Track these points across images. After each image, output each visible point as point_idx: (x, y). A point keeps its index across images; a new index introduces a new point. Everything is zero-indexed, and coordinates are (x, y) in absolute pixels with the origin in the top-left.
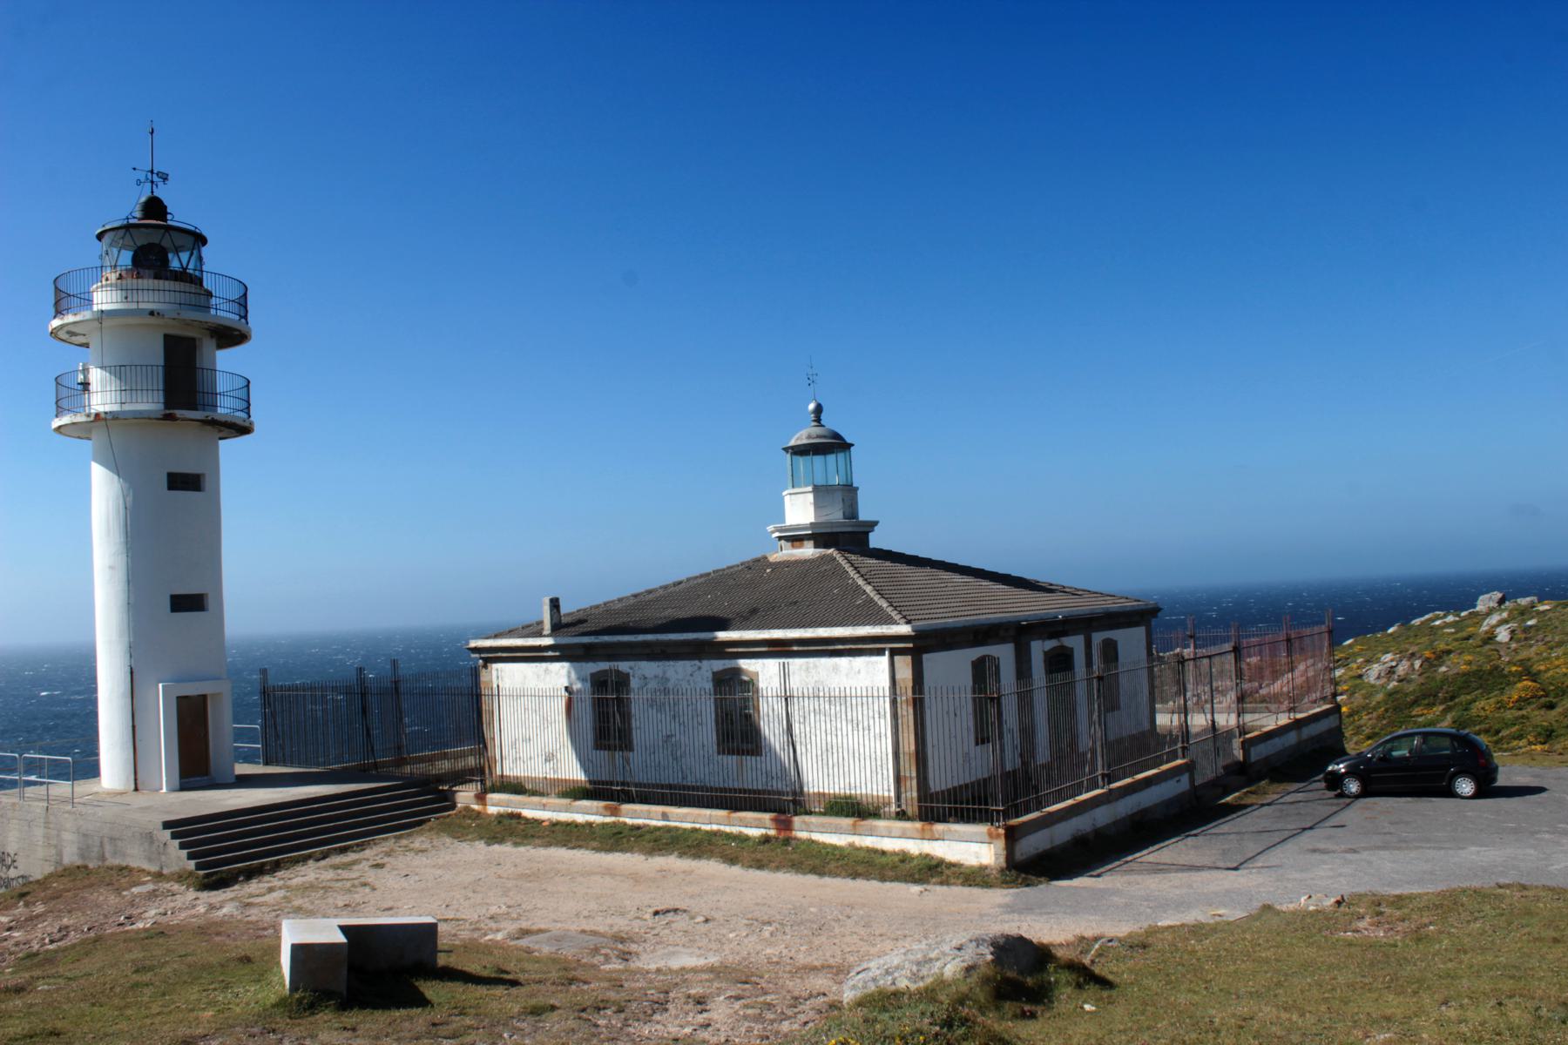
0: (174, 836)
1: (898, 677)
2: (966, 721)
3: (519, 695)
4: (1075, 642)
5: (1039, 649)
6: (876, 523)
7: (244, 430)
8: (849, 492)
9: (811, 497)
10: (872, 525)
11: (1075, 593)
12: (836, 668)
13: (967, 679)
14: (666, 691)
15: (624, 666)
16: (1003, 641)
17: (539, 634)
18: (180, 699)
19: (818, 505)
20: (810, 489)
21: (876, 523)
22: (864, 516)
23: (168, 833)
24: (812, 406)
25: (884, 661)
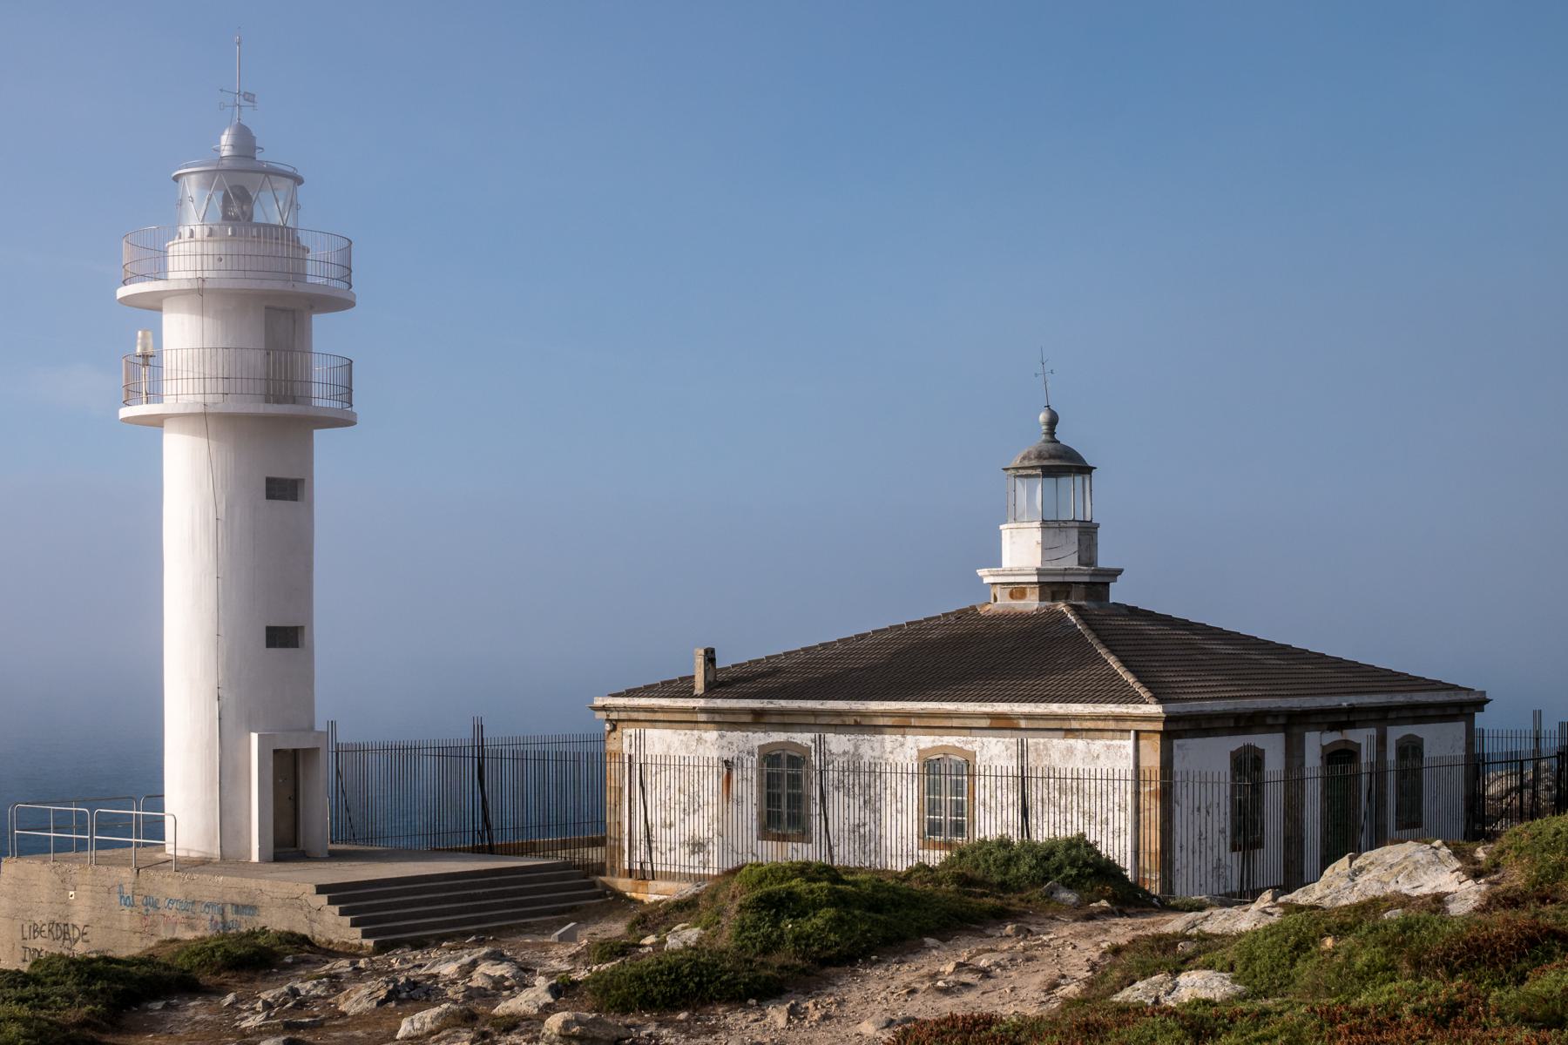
0: (331, 902)
1: (1143, 764)
2: (1221, 820)
3: (664, 764)
4: (1362, 737)
5: (1315, 743)
6: (1120, 572)
7: (346, 421)
8: (1088, 531)
9: (1037, 535)
10: (1115, 573)
11: (1454, 688)
12: (1070, 751)
13: (1224, 767)
14: (856, 771)
15: (804, 738)
16: (1271, 729)
17: (689, 693)
18: (277, 752)
19: (1046, 548)
20: (1037, 524)
21: (1120, 572)
22: (1103, 562)
23: (324, 899)
24: (1043, 417)
25: (1129, 744)
